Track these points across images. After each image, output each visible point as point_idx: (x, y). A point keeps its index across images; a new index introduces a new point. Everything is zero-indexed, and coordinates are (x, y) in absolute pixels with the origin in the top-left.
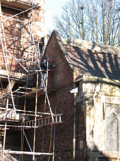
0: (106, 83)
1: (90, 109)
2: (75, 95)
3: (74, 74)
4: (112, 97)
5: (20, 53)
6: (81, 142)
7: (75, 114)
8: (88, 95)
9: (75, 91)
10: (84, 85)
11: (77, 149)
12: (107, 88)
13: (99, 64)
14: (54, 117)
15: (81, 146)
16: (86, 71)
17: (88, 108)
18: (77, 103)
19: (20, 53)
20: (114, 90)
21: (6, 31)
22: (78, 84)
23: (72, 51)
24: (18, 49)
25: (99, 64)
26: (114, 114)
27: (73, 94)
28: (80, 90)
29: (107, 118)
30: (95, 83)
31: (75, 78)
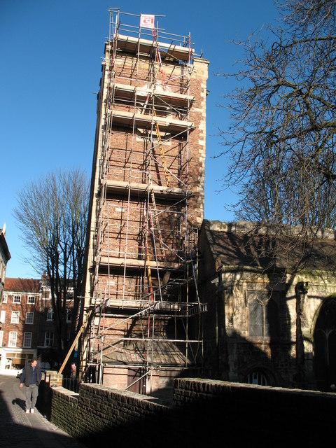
0: (247, 270)
1: (229, 298)
2: (217, 284)
3: (217, 263)
4: (254, 284)
5: (179, 242)
6: (222, 329)
7: (87, 311)
8: (226, 285)
9: (217, 281)
10: (223, 275)
11: (220, 336)
12: (248, 276)
13: (252, 248)
14: (202, 306)
15: (222, 333)
16: (235, 258)
17: (226, 296)
18: (218, 293)
19: (179, 243)
20: (256, 277)
21: (164, 222)
22: (219, 275)
23: (225, 238)
24: (178, 238)
25: (252, 248)
26: (257, 300)
27: (214, 284)
28: (220, 279)
29: (250, 305)
30: (234, 271)
31: (217, 268)
